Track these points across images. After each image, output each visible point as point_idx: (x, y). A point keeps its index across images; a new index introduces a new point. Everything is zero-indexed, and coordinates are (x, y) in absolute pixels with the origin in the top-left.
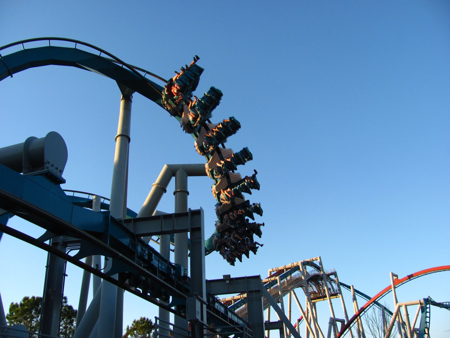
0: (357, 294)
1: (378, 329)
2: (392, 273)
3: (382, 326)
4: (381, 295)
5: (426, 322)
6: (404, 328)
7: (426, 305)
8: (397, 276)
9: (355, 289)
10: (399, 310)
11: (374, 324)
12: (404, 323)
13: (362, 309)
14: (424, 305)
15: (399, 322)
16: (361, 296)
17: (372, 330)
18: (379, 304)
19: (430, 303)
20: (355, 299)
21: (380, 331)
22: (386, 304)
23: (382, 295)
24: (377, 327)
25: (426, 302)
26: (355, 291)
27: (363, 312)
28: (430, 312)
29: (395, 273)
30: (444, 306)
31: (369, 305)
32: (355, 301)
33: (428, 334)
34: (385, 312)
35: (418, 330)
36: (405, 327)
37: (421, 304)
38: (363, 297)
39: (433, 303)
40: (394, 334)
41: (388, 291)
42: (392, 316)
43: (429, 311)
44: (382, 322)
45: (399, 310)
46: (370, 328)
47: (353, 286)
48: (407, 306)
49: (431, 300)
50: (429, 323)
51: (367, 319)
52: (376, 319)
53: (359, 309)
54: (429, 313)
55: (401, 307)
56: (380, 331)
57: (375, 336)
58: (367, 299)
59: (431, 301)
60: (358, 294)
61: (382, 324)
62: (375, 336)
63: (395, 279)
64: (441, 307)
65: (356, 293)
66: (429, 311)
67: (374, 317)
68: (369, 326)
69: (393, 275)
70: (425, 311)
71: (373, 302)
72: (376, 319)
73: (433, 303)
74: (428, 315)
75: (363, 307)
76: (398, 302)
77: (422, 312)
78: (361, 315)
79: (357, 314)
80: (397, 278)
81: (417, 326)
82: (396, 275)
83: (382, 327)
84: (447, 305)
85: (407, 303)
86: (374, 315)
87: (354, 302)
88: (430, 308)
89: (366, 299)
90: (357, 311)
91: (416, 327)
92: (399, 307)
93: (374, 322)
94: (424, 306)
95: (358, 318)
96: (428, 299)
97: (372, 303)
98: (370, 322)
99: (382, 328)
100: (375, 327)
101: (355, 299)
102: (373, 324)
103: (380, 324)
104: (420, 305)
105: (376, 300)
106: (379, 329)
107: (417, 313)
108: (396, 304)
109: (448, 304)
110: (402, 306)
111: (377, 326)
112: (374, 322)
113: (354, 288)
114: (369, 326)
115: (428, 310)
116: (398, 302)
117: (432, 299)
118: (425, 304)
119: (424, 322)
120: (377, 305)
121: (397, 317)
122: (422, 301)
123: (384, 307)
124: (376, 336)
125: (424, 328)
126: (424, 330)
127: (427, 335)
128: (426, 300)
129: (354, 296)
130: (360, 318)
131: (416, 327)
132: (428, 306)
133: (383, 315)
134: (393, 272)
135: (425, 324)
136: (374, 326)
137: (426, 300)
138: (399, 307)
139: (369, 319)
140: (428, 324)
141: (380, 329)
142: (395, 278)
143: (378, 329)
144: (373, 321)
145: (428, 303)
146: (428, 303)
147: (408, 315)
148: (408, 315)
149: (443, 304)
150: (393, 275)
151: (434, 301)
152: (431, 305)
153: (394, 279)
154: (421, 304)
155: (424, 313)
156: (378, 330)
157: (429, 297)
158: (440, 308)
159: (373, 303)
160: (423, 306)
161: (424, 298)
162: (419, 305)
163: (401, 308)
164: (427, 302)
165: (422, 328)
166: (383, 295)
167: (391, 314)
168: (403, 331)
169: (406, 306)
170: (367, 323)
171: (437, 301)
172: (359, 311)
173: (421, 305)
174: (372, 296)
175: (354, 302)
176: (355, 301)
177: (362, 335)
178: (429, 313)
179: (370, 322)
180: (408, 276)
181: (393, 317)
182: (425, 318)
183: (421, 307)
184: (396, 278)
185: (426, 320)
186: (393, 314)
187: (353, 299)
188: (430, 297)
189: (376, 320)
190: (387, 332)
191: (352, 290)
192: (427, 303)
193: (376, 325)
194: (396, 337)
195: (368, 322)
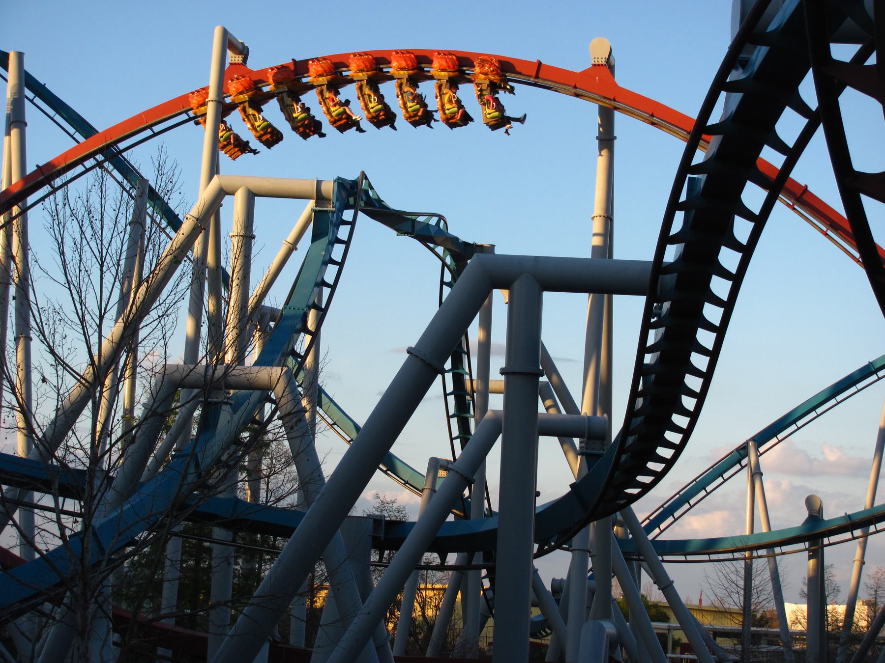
0: (32, 101)
1: (102, 266)
2: (225, 33)
3: (124, 256)
4: (150, 127)
5: (319, 280)
6: (215, 293)
7: (341, 211)
8: (243, 51)
9: (27, 73)
10: (213, 208)
11: (89, 240)
12: (220, 278)
13: (42, 174)
14: (330, 208)
15: (200, 263)
16: (51, 112)
17: (72, 268)
18: (127, 171)
19: (362, 204)
20: (16, 120)
21: (109, 278)
22: (163, 157)
23: (154, 128)
24: (97, 254)
25: (344, 194)
26: (27, 81)
27: (46, 189)
28: (341, 265)
29: (240, 37)
30: (417, 228)
31: (81, 161)
32: (14, 132)
33: (315, 336)
34: (150, 211)
35: (273, 313)
36: (224, 293)
37: (320, 198)
38: (58, 118)
39: (375, 206)
40: (168, 301)
41: (186, 112)
42: (173, 234)
43: (339, 260)
44: (127, 236)
45: (213, 208)
46: (62, 254)
47: (20, 56)
48: (256, 198)
49: (366, 192)
50: (333, 287)
51: (60, 207)
52: (102, 221)
53: (30, 169)
54: (337, 267)
55: (227, 197)
56: (109, 278)
57: (80, 297)
58: (78, 136)
59: (364, 198)
60: (38, 101)
61: (125, 247)
62: (80, 297)
63: (231, 64)
64: (401, 231)
65: (28, 93)
66: (339, 260)
67: (92, 209)
68: (61, 245)
69: (229, 43)
70: (330, 234)
71: (100, 151)
72: (102, 221)
73: (375, 206)
74: (337, 252)
75: (49, 165)
76: (218, 173)
77: (315, 238)
78: (31, 200)
79: (16, 190)
80: (245, 60)
81: (276, 299)
82: (241, 47)
83: (122, 263)
84: (428, 224)
85: (257, 183)
86: (95, 199)
87: (8, 133)
88: (352, 224)
89: (72, 130)
90: (15, 179)
91: (267, 302)
92: (222, 193)
93: (89, 233)
94: (333, 212)
95: (15, 210)
96: (355, 184)
97: (92, 155)
98: (72, 227)
99: (119, 265)
100: (87, 255)
101: (16, 120)
102: (84, 242)
103: (116, 244)
104: (316, 202)
105: (122, 145)
106: (105, 269)
107: (291, 238)
108: (211, 178)
109: (433, 221)
110: (233, 194)
111: (101, 253)
112: (89, 233)
113: (27, 67)
114: (61, 245)
115: (343, 232)
116: (218, 173)
117: (372, 188)
118: (338, 205)
119: (310, 278)
120: (116, 173)
121: (200, 238)
122: (329, 188)
123: (150, 187)
124: (83, 294)
125: (303, 305)
126: (301, 312)
127: (308, 338)
128: (349, 187)
129: (18, 105)
130: (24, 212)
131: (267, 302)
132: (348, 215)
133: (137, 223)
134: (229, 30)
135: (316, 289)
136: (86, 248)
137: (349, 187)
138: (222, 193)
139: (68, 212)
140: (326, 291)
141: (109, 268)
142: (232, 57)
143: (102, 266)
144: (86, 223)
145: (351, 200)
146: (351, 200)
147: (248, 237)
148: (248, 237)
149: (414, 218)
150: (229, 43)
151: (379, 201)
152: (360, 213)
153: (227, 65)
154: (320, 198)
155: (325, 241)
156: (101, 270)
157: (364, 176)
158: (395, 233)
159: (100, 157)
160: (326, 211)
161: (339, 178)
162: (311, 204)
163: (227, 199)
164: (349, 197)
165: (299, 303)
166: (157, 129)
167: (175, 222)
168: (209, 304)
169: (251, 196)
170: (56, 227)
171: (394, 202)
172: (24, 177)
173: (317, 205)
174: (102, 122)
175: (8, 133)
176: (14, 132)
177: (16, 280)
178: (337, 267)
179: (72, 227)
180: (293, 60)
181: (179, 237)
182: (320, 262)
183: (316, 212)
184: (238, 59)
185: (322, 272)
186: (183, 226)
187: (8, 117)
188: (366, 178)
189: (98, 224)
190: (138, 287)
191: (12, 74)
192: (348, 201)
193: (93, 244)
194: (173, 315)
195: (59, 223)
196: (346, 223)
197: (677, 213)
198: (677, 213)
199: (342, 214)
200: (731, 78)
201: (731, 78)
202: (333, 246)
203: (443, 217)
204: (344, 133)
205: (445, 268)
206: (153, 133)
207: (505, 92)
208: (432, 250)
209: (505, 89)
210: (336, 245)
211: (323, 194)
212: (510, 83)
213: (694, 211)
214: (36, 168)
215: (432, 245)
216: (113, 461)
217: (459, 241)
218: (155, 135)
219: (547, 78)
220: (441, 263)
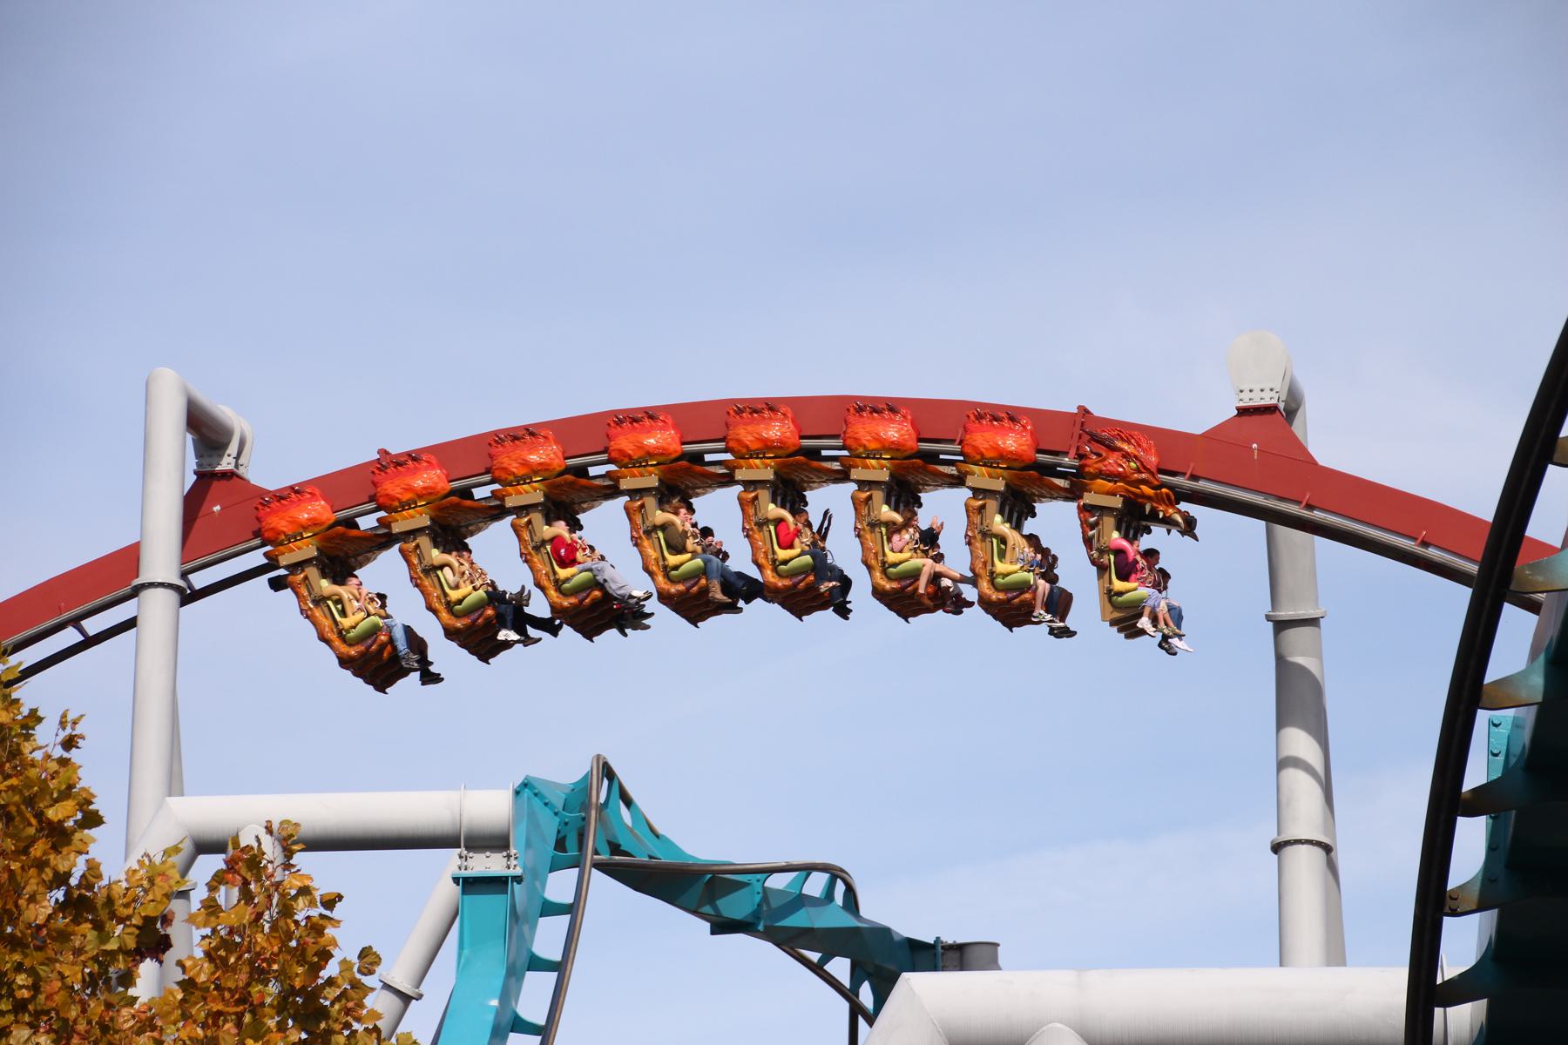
88: (573, 910)
152: (597, 875)
196: (550, 909)
197: (1463, 823)
198: (1463, 823)
199: (544, 885)
200: (389, 647)
201: (389, 647)
202: (520, 978)
203: (842, 871)
204: (595, 639)
205: (861, 1020)
206: (82, 638)
207: (1169, 531)
208: (818, 969)
209: (1168, 522)
210: (531, 976)
211: (1286, 631)
212: (1183, 506)
213: (1514, 812)
214: (699, 624)
215: (814, 956)
216: (1515, 756)
217: (892, 938)
218: (89, 642)
219: (1286, 496)
220: (844, 1006)
